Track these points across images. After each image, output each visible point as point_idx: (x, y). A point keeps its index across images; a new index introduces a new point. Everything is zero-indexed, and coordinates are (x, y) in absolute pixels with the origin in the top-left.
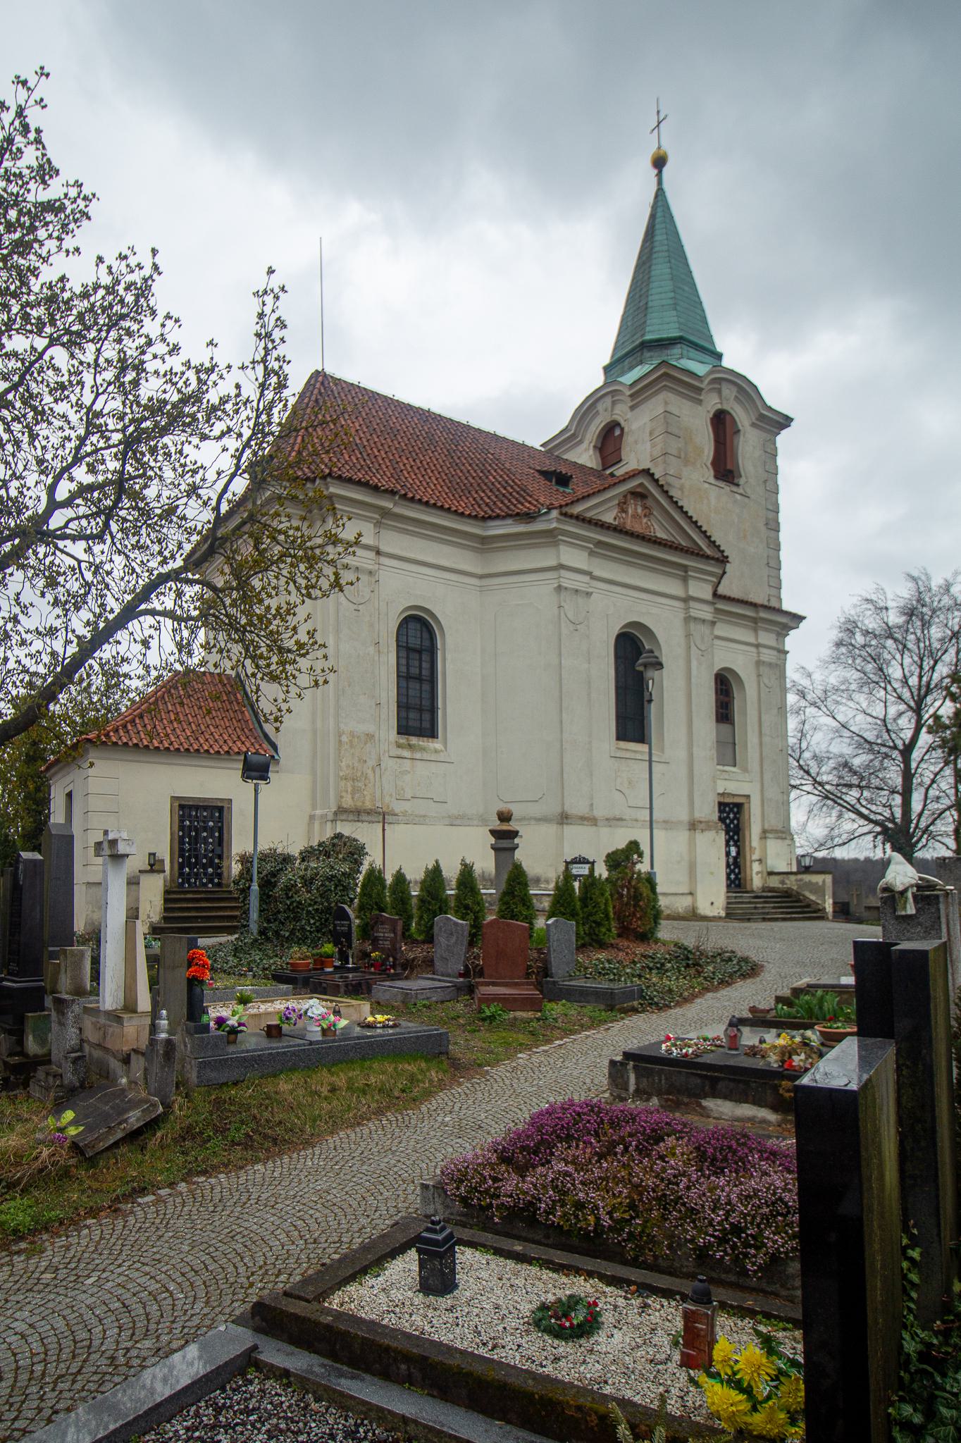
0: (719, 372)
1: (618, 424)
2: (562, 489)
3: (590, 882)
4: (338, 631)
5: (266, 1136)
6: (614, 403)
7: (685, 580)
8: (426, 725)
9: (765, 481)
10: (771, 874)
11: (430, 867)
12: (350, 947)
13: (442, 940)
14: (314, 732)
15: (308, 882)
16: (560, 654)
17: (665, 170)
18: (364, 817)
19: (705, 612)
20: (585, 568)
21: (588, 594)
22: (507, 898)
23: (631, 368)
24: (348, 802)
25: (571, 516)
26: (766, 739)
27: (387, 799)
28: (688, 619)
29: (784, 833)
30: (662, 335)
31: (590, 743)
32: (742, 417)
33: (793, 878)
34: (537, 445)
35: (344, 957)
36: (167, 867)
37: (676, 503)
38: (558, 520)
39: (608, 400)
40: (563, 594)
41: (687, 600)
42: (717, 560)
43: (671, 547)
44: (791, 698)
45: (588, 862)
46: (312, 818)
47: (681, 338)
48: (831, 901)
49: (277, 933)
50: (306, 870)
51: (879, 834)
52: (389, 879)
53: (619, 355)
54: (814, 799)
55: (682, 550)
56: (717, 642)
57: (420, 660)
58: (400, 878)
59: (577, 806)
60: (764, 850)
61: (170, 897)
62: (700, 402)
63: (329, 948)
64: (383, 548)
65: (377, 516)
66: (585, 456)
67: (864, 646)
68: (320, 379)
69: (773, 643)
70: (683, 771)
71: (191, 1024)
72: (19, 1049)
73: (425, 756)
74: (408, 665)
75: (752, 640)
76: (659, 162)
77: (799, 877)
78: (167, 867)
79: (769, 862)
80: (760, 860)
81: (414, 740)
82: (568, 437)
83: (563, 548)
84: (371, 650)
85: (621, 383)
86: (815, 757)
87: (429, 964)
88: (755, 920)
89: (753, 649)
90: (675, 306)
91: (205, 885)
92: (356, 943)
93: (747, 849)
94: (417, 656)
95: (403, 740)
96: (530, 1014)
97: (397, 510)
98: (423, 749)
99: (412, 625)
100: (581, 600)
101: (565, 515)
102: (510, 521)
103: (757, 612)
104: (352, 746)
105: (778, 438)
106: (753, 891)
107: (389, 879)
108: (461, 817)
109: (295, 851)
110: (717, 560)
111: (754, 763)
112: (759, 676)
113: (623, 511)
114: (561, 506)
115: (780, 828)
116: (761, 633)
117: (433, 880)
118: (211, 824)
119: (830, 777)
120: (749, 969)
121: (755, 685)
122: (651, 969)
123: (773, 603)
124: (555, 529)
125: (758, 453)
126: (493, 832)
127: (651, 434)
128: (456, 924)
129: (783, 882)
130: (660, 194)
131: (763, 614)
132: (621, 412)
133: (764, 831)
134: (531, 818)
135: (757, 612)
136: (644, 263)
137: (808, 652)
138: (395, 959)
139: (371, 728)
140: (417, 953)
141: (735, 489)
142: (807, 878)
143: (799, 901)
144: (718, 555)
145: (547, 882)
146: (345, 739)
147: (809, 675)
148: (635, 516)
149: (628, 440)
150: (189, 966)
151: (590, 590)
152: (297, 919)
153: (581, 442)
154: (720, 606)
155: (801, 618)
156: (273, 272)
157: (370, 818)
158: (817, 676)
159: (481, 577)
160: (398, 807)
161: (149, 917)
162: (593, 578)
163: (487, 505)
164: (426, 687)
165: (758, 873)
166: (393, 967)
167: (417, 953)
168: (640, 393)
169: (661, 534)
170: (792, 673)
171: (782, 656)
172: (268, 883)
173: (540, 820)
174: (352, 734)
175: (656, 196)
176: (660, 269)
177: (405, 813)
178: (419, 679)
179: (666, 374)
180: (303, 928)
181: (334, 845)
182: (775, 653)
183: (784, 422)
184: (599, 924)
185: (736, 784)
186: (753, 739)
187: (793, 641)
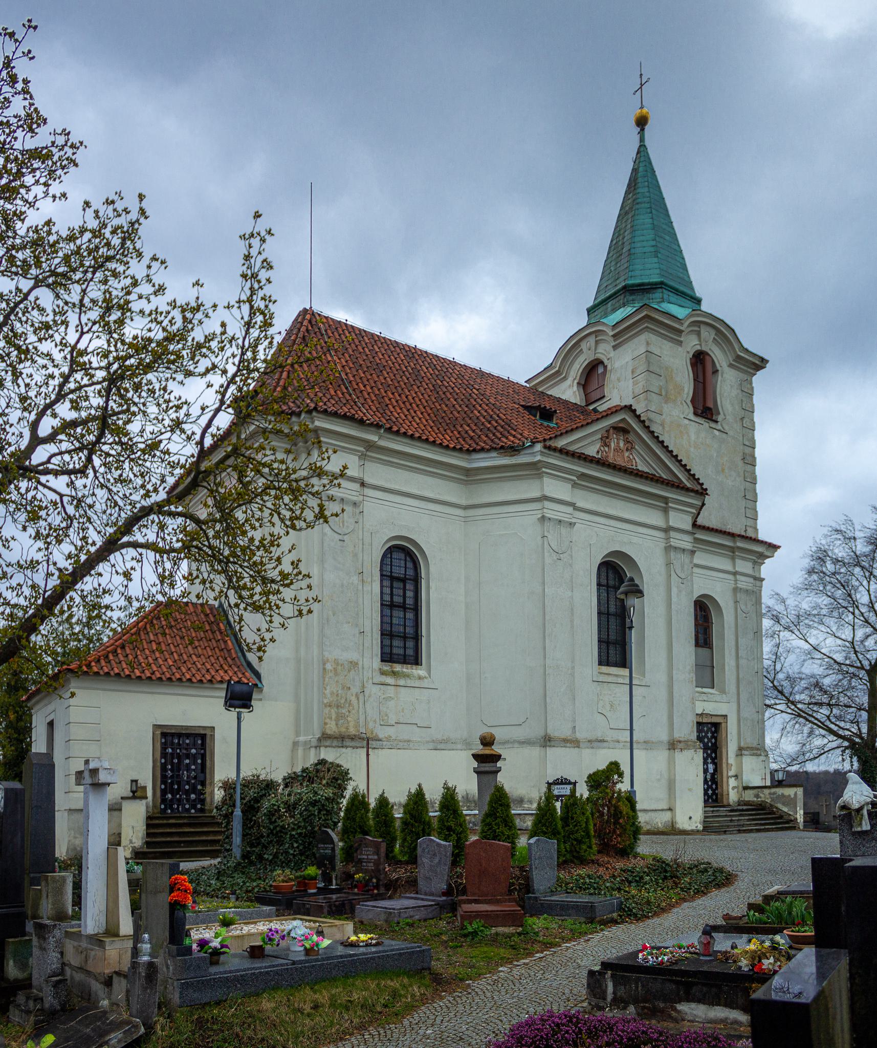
0: (698, 315)
1: (602, 362)
2: (546, 424)
4: (322, 561)
6: (597, 342)
7: (666, 511)
8: (410, 652)
9: (742, 419)
10: (746, 788)
11: (413, 791)
12: (333, 869)
13: (425, 860)
14: (298, 661)
15: (291, 808)
16: (544, 583)
17: (646, 127)
18: (348, 743)
19: (685, 542)
21: (572, 525)
23: (614, 310)
24: (332, 728)
26: (742, 662)
27: (371, 725)
28: (669, 548)
29: (759, 750)
30: (643, 278)
31: (573, 668)
32: (719, 357)
33: (767, 791)
35: (327, 879)
36: (150, 793)
38: (542, 453)
39: (592, 340)
40: (547, 524)
41: (667, 530)
42: (697, 492)
44: (767, 623)
45: (570, 783)
46: (295, 744)
47: (662, 283)
48: (802, 812)
49: (260, 858)
50: (289, 795)
51: (846, 748)
52: (373, 803)
53: (603, 297)
56: (696, 570)
57: (404, 589)
58: (383, 802)
59: (559, 729)
61: (152, 822)
62: (680, 343)
63: (312, 870)
64: (368, 480)
65: (362, 449)
67: (834, 574)
68: (308, 317)
69: (749, 571)
70: (662, 694)
73: (409, 682)
74: (392, 595)
75: (730, 568)
76: (642, 122)
77: (773, 790)
78: (150, 793)
80: (736, 776)
81: (398, 668)
82: (553, 374)
84: (355, 579)
86: (788, 677)
87: (412, 884)
88: (731, 833)
89: (731, 577)
90: (656, 254)
91: (188, 811)
92: (339, 865)
93: (724, 766)
94: (401, 585)
95: (386, 667)
96: (511, 930)
97: (383, 443)
99: (395, 555)
100: (564, 530)
101: (549, 448)
102: (494, 454)
103: (735, 542)
104: (336, 674)
105: (754, 378)
106: (729, 805)
107: (373, 803)
108: (445, 741)
109: (278, 776)
110: (697, 492)
111: (731, 687)
112: (736, 602)
113: (606, 445)
117: (416, 803)
118: (193, 751)
121: (732, 611)
122: (630, 882)
123: (750, 533)
124: (540, 461)
125: (735, 392)
126: (476, 757)
127: (633, 372)
129: (757, 796)
130: (642, 150)
131: (740, 544)
132: (604, 351)
133: (740, 749)
134: (514, 742)
135: (735, 542)
137: (782, 576)
138: (378, 880)
139: (353, 656)
141: (713, 425)
142: (780, 791)
145: (531, 802)
146: (329, 666)
147: (783, 601)
149: (611, 378)
151: (574, 520)
152: (280, 843)
153: (565, 379)
154: (700, 535)
155: (775, 547)
156: (260, 216)
158: (791, 602)
159: (466, 508)
160: (382, 733)
161: (131, 842)
164: (410, 615)
165: (734, 788)
166: (377, 887)
168: (622, 334)
169: (642, 467)
171: (758, 583)
172: (250, 809)
173: (523, 743)
174: (336, 662)
175: (632, 185)
176: (644, 219)
177: (388, 739)
178: (403, 607)
180: (287, 853)
181: (318, 771)
182: (751, 580)
183: (759, 364)
184: (580, 842)
185: (714, 705)
187: (768, 568)
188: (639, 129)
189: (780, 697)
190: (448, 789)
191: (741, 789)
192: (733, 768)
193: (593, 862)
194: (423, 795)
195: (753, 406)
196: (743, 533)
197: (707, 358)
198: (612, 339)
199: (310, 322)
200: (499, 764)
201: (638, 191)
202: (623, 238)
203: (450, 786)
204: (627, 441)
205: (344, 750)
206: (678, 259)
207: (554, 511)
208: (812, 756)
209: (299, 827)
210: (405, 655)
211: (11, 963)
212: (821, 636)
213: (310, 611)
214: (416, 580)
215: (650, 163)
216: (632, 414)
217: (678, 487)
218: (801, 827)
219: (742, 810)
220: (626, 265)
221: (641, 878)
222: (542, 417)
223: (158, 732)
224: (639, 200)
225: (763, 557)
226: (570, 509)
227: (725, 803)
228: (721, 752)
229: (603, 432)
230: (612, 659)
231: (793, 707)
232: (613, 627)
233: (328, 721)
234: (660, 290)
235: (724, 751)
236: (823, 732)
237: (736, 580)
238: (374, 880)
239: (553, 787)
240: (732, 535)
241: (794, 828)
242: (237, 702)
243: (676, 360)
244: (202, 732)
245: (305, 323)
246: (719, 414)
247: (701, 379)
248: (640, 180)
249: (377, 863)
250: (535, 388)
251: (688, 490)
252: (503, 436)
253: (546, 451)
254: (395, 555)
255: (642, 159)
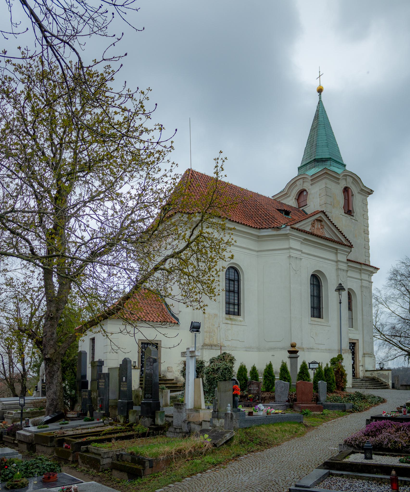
0: (346, 172)
1: (306, 190)
2: (287, 217)
3: (327, 370)
5: (265, 443)
7: (336, 254)
8: (236, 310)
10: (366, 371)
11: (268, 364)
16: (290, 283)
17: (322, 93)
18: (214, 347)
19: (344, 266)
20: (299, 249)
22: (301, 374)
23: (310, 169)
24: (207, 342)
25: (295, 229)
28: (338, 269)
29: (371, 355)
32: (354, 189)
34: (270, 197)
37: (334, 224)
39: (301, 181)
41: (337, 262)
42: (349, 246)
43: (332, 241)
44: (374, 301)
45: (317, 363)
47: (330, 158)
48: (391, 381)
51: (407, 355)
54: (381, 341)
55: (336, 242)
56: (348, 278)
57: (234, 284)
58: (254, 369)
60: (364, 361)
62: (339, 183)
66: (291, 202)
67: (401, 281)
68: (191, 172)
69: (367, 279)
71: (235, 409)
72: (153, 423)
73: (237, 323)
74: (229, 286)
75: (359, 277)
79: (366, 366)
81: (232, 317)
82: (284, 194)
83: (291, 241)
85: (307, 174)
86: (382, 325)
89: (360, 281)
93: (358, 361)
94: (233, 283)
95: (228, 316)
96: (319, 413)
98: (235, 320)
99: (231, 270)
101: (293, 228)
102: (270, 230)
103: (361, 266)
105: (368, 198)
106: (360, 378)
110: (349, 246)
111: (360, 328)
112: (362, 292)
113: (313, 226)
114: (291, 225)
115: (370, 353)
116: (363, 275)
117: (269, 368)
119: (387, 333)
120: (383, 401)
122: (350, 400)
123: (367, 263)
126: (289, 351)
127: (319, 195)
128: (285, 383)
129: (372, 374)
130: (320, 102)
131: (364, 267)
132: (307, 186)
133: (364, 354)
135: (361, 266)
136: (314, 128)
137: (380, 283)
138: (259, 397)
140: (265, 395)
141: (352, 217)
143: (378, 382)
144: (349, 244)
147: (379, 292)
148: (318, 229)
149: (310, 197)
150: (233, 391)
151: (301, 257)
153: (289, 196)
154: (350, 264)
155: (378, 269)
156: (221, 152)
157: (216, 348)
158: (383, 292)
159: (258, 251)
162: (302, 253)
163: (260, 223)
164: (236, 295)
165: (361, 371)
166: (258, 400)
167: (265, 395)
168: (315, 179)
169: (327, 236)
170: (373, 292)
173: (282, 349)
178: (234, 292)
179: (326, 173)
181: (223, 356)
182: (368, 282)
183: (370, 192)
185: (355, 335)
186: (359, 317)
187: (374, 278)
188: (319, 94)
189: (378, 333)
190: (283, 363)
191: (364, 371)
192: (361, 362)
193: (335, 392)
194: (272, 365)
195: (368, 209)
196: (364, 263)
197: (349, 190)
198: (310, 181)
199: (192, 174)
200: (298, 354)
201: (320, 119)
202: (313, 139)
203: (284, 362)
204: (321, 225)
205: (212, 350)
206: (336, 148)
207: (294, 254)
208: (391, 358)
209: (220, 378)
210: (234, 312)
211: (159, 419)
212: (396, 307)
213: (219, 295)
214: (239, 281)
215: (324, 108)
216: (318, 211)
217: (342, 244)
218: (391, 388)
219: (366, 380)
220: (315, 150)
221: (354, 398)
222: (285, 214)
223: (140, 342)
224: (320, 123)
225: (372, 273)
226: (300, 253)
227: (358, 377)
228: (356, 355)
229: (312, 221)
230: (315, 314)
231: (383, 337)
232: (315, 301)
233: (206, 338)
234: (329, 161)
235: (357, 355)
236: (395, 348)
237: (362, 283)
238: (257, 397)
239: (311, 365)
240: (361, 264)
241: (388, 388)
242: (195, 330)
243: (337, 191)
244: (157, 342)
245: (190, 175)
246: (354, 213)
247: (347, 198)
248: (320, 115)
249: (258, 391)
250: (275, 200)
251: (345, 245)
252: (273, 222)
253: (291, 229)
254: (231, 270)
255: (321, 106)
